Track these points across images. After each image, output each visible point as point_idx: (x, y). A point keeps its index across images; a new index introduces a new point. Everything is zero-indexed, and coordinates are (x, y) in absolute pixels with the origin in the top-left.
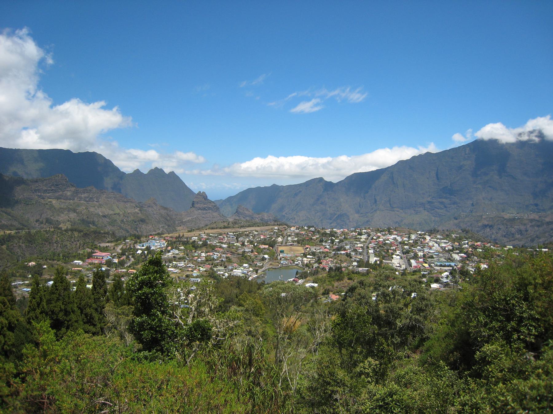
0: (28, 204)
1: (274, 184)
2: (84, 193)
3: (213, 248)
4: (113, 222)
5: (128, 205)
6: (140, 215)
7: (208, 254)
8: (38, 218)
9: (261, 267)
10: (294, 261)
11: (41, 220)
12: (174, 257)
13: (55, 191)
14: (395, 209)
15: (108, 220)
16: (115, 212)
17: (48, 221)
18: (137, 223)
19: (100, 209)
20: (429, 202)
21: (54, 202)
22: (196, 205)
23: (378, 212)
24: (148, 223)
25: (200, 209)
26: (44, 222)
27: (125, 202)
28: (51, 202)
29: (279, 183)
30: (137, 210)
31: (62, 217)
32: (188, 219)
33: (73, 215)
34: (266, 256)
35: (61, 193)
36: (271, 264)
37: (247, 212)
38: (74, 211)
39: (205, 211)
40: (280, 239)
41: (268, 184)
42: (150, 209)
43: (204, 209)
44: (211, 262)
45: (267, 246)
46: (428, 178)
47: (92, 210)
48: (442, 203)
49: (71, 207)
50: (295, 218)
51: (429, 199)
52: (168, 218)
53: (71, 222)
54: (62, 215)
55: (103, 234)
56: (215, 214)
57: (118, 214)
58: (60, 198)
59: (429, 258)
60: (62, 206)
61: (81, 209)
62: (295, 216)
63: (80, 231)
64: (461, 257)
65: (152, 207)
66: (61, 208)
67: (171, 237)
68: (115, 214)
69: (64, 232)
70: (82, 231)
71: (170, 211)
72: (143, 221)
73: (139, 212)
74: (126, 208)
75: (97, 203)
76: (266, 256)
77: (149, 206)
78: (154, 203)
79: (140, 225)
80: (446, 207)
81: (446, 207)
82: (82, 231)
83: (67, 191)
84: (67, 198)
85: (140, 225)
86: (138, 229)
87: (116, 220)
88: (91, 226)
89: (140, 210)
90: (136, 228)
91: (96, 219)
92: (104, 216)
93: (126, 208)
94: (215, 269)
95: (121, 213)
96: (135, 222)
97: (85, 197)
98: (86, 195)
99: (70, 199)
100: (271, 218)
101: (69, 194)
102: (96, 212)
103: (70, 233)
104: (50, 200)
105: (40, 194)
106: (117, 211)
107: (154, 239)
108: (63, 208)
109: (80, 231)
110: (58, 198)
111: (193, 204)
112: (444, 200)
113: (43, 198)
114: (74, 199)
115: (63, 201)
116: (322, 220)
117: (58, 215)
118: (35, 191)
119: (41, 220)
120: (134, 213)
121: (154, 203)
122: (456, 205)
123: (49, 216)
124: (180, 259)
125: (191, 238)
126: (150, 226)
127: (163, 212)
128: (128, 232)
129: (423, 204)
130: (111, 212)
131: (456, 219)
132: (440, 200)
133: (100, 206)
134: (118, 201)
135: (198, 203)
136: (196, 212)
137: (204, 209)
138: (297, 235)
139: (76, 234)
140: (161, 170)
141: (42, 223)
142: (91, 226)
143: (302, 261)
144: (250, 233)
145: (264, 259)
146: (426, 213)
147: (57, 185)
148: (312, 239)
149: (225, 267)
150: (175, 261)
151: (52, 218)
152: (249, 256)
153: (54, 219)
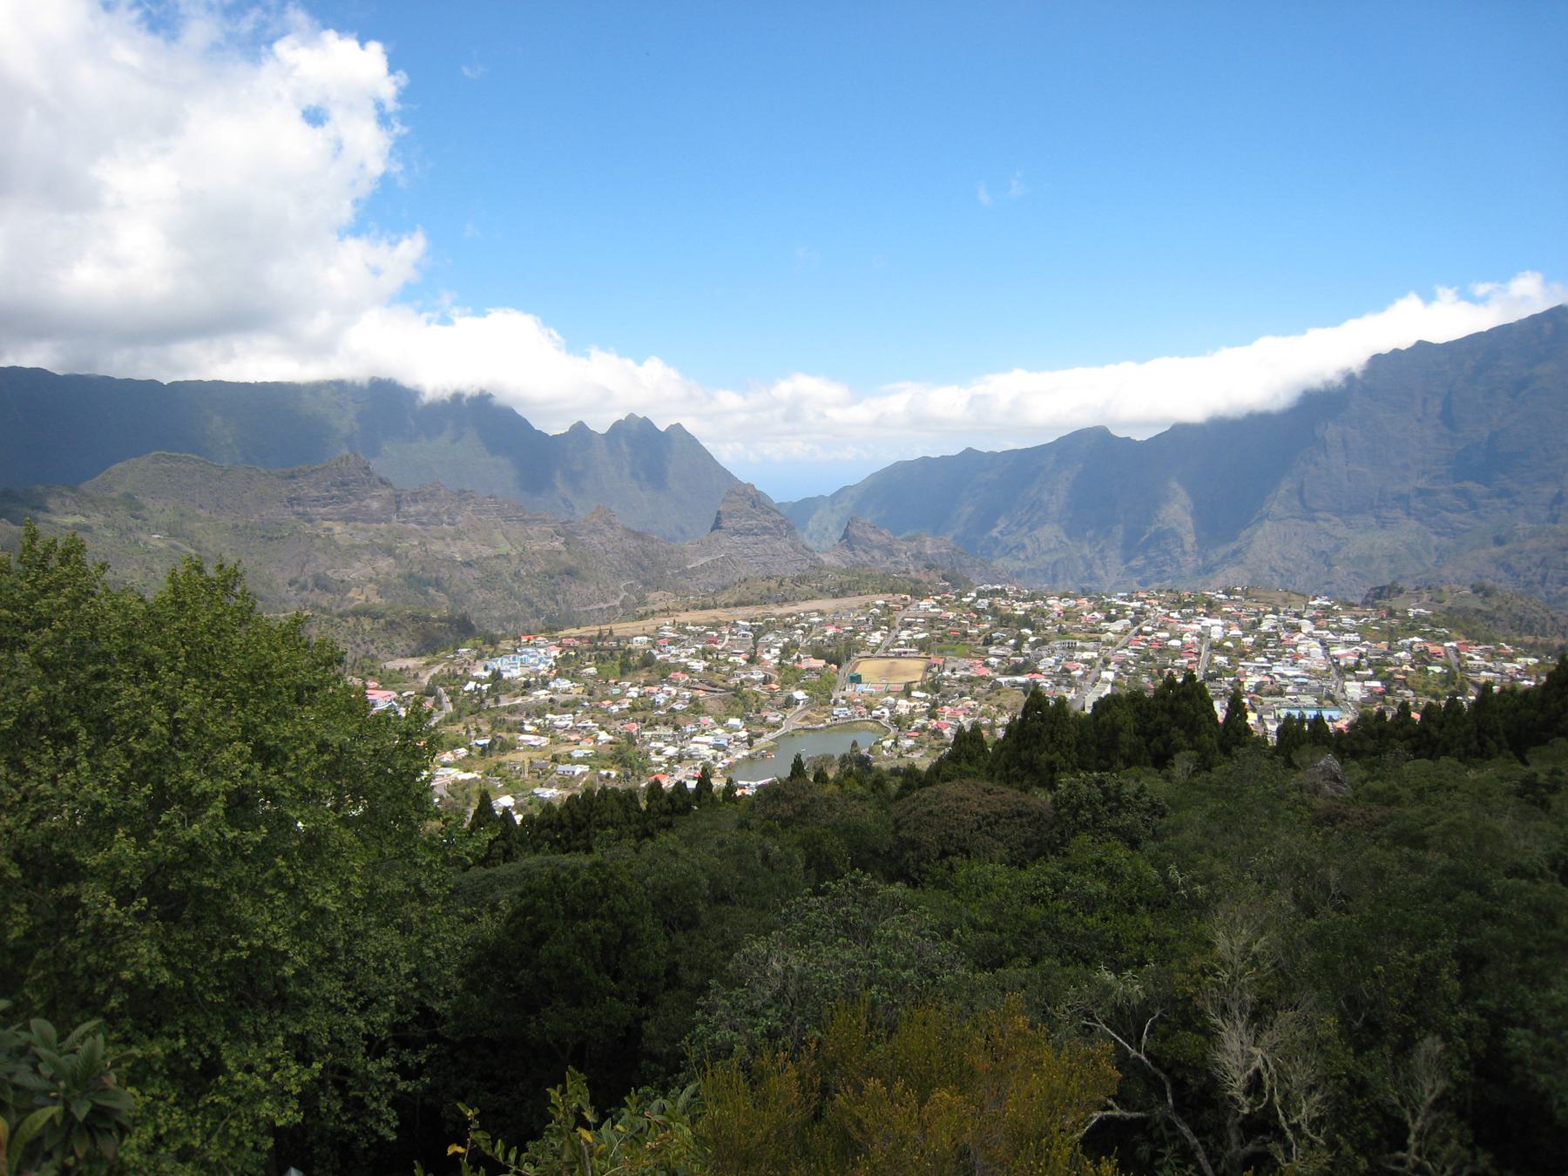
0: (271, 539)
1: (969, 449)
2: (416, 501)
3: (664, 672)
4: (490, 580)
5: (534, 530)
6: (564, 557)
7: (647, 689)
8: (295, 575)
9: (776, 726)
10: (869, 708)
11: (302, 580)
12: (551, 700)
13: (343, 500)
14: (1321, 515)
15: (478, 574)
16: (497, 552)
17: (322, 584)
18: (557, 578)
19: (459, 543)
20: (1421, 492)
21: (338, 528)
22: (726, 523)
23: (1267, 524)
24: (586, 580)
25: (737, 532)
26: (310, 586)
27: (526, 522)
28: (330, 529)
29: (985, 446)
30: (557, 544)
31: (356, 571)
32: (702, 561)
33: (385, 564)
34: (799, 694)
35: (355, 504)
36: (807, 718)
37: (873, 537)
38: (389, 552)
39: (751, 539)
40: (876, 637)
41: (953, 450)
42: (596, 539)
43: (749, 532)
44: (640, 715)
45: (821, 663)
46: (1419, 420)
47: (437, 546)
48: (1464, 494)
49: (380, 541)
50: (1024, 547)
51: (1422, 483)
52: (646, 562)
53: (377, 582)
54: (358, 565)
55: (435, 621)
56: (781, 545)
57: (506, 556)
58: (356, 520)
59: (1270, 694)
60: (357, 541)
61: (410, 545)
62: (1026, 541)
63: (375, 617)
64: (1370, 690)
65: (601, 532)
66: (353, 546)
67: (580, 638)
68: (497, 557)
69: (337, 620)
70: (383, 616)
71: (652, 541)
72: (570, 573)
73: (563, 548)
74: (529, 538)
75: (451, 528)
76: (799, 694)
77: (593, 531)
78: (609, 523)
79: (564, 585)
80: (1474, 506)
81: (1474, 506)
82: (383, 616)
83: (373, 497)
84: (371, 518)
85: (564, 585)
86: (559, 597)
87: (499, 574)
88: (432, 591)
89: (566, 543)
90: (555, 593)
91: (445, 573)
92: (468, 564)
93: (529, 538)
94: (648, 734)
95: (513, 553)
96: (552, 577)
97: (418, 514)
98: (421, 507)
99: (379, 521)
100: (943, 550)
101: (375, 505)
102: (448, 552)
103: (351, 621)
104: (327, 524)
105: (301, 509)
106: (505, 548)
107: (534, 645)
108: (358, 547)
109: (375, 617)
110: (347, 519)
111: (718, 520)
112: (1469, 485)
113: (310, 521)
114: (388, 521)
115: (360, 525)
116: (1102, 551)
117: (347, 565)
118: (290, 500)
119: (302, 580)
120: (549, 552)
121: (609, 523)
122: (1506, 500)
123: (321, 570)
124: (569, 706)
125: (628, 639)
126: (593, 588)
127: (631, 544)
128: (531, 604)
129: (1401, 498)
130: (487, 552)
131: (1499, 541)
132: (1458, 486)
133: (458, 535)
134: (507, 519)
135: (730, 515)
136: (726, 542)
137: (749, 532)
138: (932, 622)
139: (367, 624)
140: (646, 424)
141: (304, 587)
142: (432, 591)
143: (892, 707)
144: (799, 619)
145: (790, 703)
146: (1413, 524)
147: (344, 484)
148: (965, 634)
149: (676, 729)
150: (552, 711)
151: (329, 573)
152: (755, 694)
153: (336, 576)
